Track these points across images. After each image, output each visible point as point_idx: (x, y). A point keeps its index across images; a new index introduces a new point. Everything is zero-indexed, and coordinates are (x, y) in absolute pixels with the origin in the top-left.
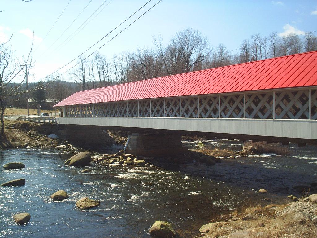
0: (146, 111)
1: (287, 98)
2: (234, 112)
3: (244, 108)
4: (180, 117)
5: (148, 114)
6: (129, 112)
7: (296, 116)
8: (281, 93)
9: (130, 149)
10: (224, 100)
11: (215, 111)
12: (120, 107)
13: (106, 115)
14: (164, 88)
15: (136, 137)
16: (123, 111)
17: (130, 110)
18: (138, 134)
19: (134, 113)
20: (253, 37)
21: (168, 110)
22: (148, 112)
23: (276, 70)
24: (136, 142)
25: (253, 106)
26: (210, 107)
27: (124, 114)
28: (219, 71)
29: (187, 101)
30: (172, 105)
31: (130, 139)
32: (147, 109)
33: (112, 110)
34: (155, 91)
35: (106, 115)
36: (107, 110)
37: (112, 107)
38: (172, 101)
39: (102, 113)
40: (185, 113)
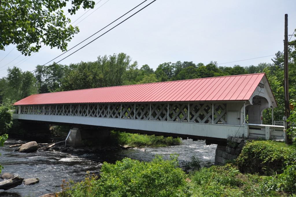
0: (85, 112)
1: (158, 108)
2: (178, 117)
3: (150, 113)
4: (262, 123)
5: (94, 114)
6: (72, 112)
7: (203, 120)
8: (156, 105)
9: (71, 140)
10: (153, 107)
11: (163, 115)
12: (66, 108)
13: (67, 114)
14: (125, 97)
15: (76, 131)
16: (67, 111)
17: (73, 110)
18: (78, 129)
19: (83, 113)
20: (65, 65)
21: (111, 112)
22: (86, 112)
23: (166, 88)
24: (75, 134)
25: (141, 111)
26: (196, 113)
27: (68, 113)
28: (134, 87)
29: (147, 106)
30: (103, 108)
31: (71, 132)
32: (95, 110)
33: (59, 110)
34: (112, 98)
35: (67, 114)
36: (55, 110)
37: (59, 107)
38: (103, 105)
39: (57, 112)
40: (118, 114)
